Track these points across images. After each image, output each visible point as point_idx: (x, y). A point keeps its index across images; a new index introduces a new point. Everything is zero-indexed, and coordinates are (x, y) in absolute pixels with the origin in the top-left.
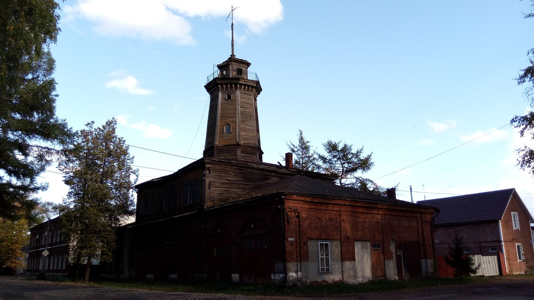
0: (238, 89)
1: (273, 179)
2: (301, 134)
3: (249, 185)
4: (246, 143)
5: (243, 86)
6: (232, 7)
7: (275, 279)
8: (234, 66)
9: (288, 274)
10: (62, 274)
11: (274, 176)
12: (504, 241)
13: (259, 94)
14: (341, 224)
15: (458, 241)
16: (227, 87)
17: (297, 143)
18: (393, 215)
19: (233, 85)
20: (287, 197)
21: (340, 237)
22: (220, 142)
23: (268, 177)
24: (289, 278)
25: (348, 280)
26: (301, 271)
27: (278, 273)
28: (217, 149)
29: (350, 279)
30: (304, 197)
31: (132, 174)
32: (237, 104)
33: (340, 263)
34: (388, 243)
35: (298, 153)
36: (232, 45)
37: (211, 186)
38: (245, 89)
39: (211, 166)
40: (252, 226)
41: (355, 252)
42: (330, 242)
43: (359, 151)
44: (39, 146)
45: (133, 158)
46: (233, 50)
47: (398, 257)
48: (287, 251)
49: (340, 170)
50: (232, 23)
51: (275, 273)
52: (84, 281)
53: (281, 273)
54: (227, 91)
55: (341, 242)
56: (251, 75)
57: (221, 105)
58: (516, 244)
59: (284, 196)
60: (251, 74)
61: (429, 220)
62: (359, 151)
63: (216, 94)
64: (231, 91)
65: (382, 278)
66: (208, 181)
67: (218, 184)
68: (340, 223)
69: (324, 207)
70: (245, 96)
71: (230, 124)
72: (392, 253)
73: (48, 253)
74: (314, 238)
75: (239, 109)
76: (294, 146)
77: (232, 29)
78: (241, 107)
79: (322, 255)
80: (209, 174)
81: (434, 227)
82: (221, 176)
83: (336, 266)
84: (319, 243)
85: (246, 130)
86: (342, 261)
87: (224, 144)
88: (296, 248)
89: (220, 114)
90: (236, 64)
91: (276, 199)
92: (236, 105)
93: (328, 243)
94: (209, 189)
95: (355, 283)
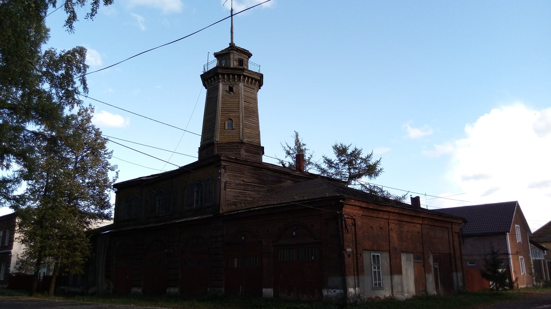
0: (241, 81)
2: (297, 136)
5: (247, 78)
7: (329, 296)
12: (511, 254)
14: (390, 234)
16: (229, 78)
17: (293, 145)
18: (431, 225)
19: (236, 76)
20: (346, 201)
21: (388, 248)
24: (349, 294)
25: (397, 296)
26: (358, 286)
27: (333, 289)
28: (217, 147)
30: (361, 202)
31: (109, 170)
32: (240, 98)
33: (389, 277)
35: (294, 156)
36: (232, 32)
37: (227, 187)
38: (252, 83)
40: (294, 234)
41: (401, 265)
45: (112, 152)
47: (435, 269)
48: (346, 263)
49: (346, 176)
50: (232, 8)
51: (329, 288)
52: (48, 295)
53: (338, 288)
54: (228, 82)
55: (390, 253)
56: (252, 66)
57: (222, 98)
58: (520, 257)
59: (342, 201)
60: (254, 65)
61: (458, 231)
64: (234, 82)
66: (223, 180)
68: (389, 233)
69: (375, 215)
70: (248, 89)
71: (233, 119)
75: (243, 104)
76: (290, 148)
78: (244, 101)
79: (375, 268)
80: (224, 173)
81: (463, 237)
82: (236, 176)
83: (386, 280)
85: (250, 127)
88: (353, 259)
89: (220, 107)
90: (237, 53)
91: (333, 203)
92: (239, 98)
93: (379, 254)
94: (224, 190)
95: (403, 299)
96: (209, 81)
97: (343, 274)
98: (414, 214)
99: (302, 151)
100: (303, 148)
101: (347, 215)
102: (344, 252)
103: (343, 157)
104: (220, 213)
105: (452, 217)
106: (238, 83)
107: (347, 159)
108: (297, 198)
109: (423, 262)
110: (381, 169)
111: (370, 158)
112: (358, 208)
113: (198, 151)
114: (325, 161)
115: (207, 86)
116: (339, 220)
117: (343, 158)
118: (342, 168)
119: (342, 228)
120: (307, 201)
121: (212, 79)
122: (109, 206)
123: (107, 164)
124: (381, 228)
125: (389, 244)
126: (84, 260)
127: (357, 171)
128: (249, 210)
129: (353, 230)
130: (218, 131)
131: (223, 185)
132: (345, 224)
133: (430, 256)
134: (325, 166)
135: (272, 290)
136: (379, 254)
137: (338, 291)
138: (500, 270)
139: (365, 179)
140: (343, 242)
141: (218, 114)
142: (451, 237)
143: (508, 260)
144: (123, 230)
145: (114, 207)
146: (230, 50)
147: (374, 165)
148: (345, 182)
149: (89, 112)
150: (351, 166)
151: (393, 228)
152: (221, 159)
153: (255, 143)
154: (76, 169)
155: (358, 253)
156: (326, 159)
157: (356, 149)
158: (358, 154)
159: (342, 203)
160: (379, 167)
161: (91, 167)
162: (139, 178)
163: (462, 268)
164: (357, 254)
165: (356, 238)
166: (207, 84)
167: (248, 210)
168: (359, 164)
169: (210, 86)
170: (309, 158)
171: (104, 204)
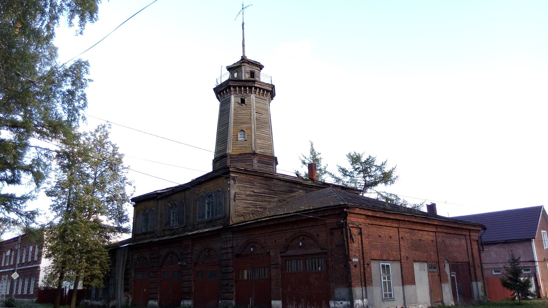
1: (299, 192)
2: (312, 145)
3: (275, 197)
4: (262, 152)
5: (258, 90)
6: (243, 5)
8: (247, 68)
9: (355, 302)
10: (30, 300)
11: (300, 189)
12: (538, 262)
13: (272, 99)
15: (515, 261)
16: (240, 91)
17: (308, 155)
19: (247, 88)
20: (350, 210)
21: (399, 256)
22: (234, 150)
23: (294, 190)
24: (356, 306)
26: (366, 298)
27: (339, 300)
29: (412, 306)
30: (367, 210)
31: (127, 185)
32: (252, 109)
33: (401, 288)
34: (443, 265)
36: (243, 45)
37: (237, 198)
38: (263, 94)
39: (236, 175)
40: (301, 244)
42: (391, 263)
43: (384, 163)
44: (38, 147)
46: (244, 51)
47: (453, 279)
48: (352, 274)
49: (362, 184)
50: (243, 22)
51: (335, 300)
53: (344, 300)
54: (240, 94)
55: (401, 262)
57: (234, 110)
61: (477, 238)
62: (384, 163)
63: (228, 98)
65: (440, 304)
66: (233, 192)
67: (244, 196)
68: (399, 242)
71: (245, 130)
72: (447, 275)
73: (19, 276)
74: (376, 259)
75: (254, 115)
77: (243, 29)
78: (256, 113)
79: (384, 278)
81: (482, 244)
84: (381, 264)
86: (403, 285)
87: (238, 153)
88: (360, 270)
91: (337, 212)
92: (251, 110)
93: (389, 264)
96: (222, 94)
97: (349, 285)
98: (427, 222)
99: (317, 160)
100: (318, 157)
101: (352, 224)
102: (350, 263)
103: (357, 165)
104: (230, 224)
105: (468, 224)
106: (249, 94)
107: (361, 168)
108: (303, 208)
109: (438, 271)
110: (397, 177)
111: (385, 165)
112: (364, 217)
113: (212, 163)
114: (340, 169)
115: (220, 99)
116: (344, 229)
117: (357, 166)
118: (356, 177)
119: (347, 237)
120: (313, 211)
121: (224, 92)
122: (127, 220)
123: (125, 179)
124: (391, 237)
125: (400, 253)
126: (103, 273)
127: (373, 179)
128: (257, 221)
129: (360, 240)
130: (231, 143)
131: (232, 196)
132: (350, 233)
133: (446, 265)
134: (339, 175)
135: (281, 302)
136: (389, 264)
137: (345, 303)
138: (522, 279)
139: (381, 187)
140: (349, 252)
141: (230, 126)
142: (469, 245)
143: (535, 267)
144: (140, 243)
145: (131, 221)
146: (241, 63)
147: (389, 172)
148: (360, 191)
149: (106, 128)
150: (366, 174)
151: (403, 237)
152: (230, 170)
153: (268, 153)
154: (95, 184)
155: (366, 263)
156: (341, 169)
157: (370, 157)
158: (372, 162)
159: (346, 212)
160: (394, 175)
161: (109, 182)
162: (155, 191)
163: (483, 277)
164: (364, 264)
165: (362, 247)
166: (220, 98)
167: (255, 221)
168: (374, 172)
169: (223, 99)
170: (325, 168)
171: (121, 218)
